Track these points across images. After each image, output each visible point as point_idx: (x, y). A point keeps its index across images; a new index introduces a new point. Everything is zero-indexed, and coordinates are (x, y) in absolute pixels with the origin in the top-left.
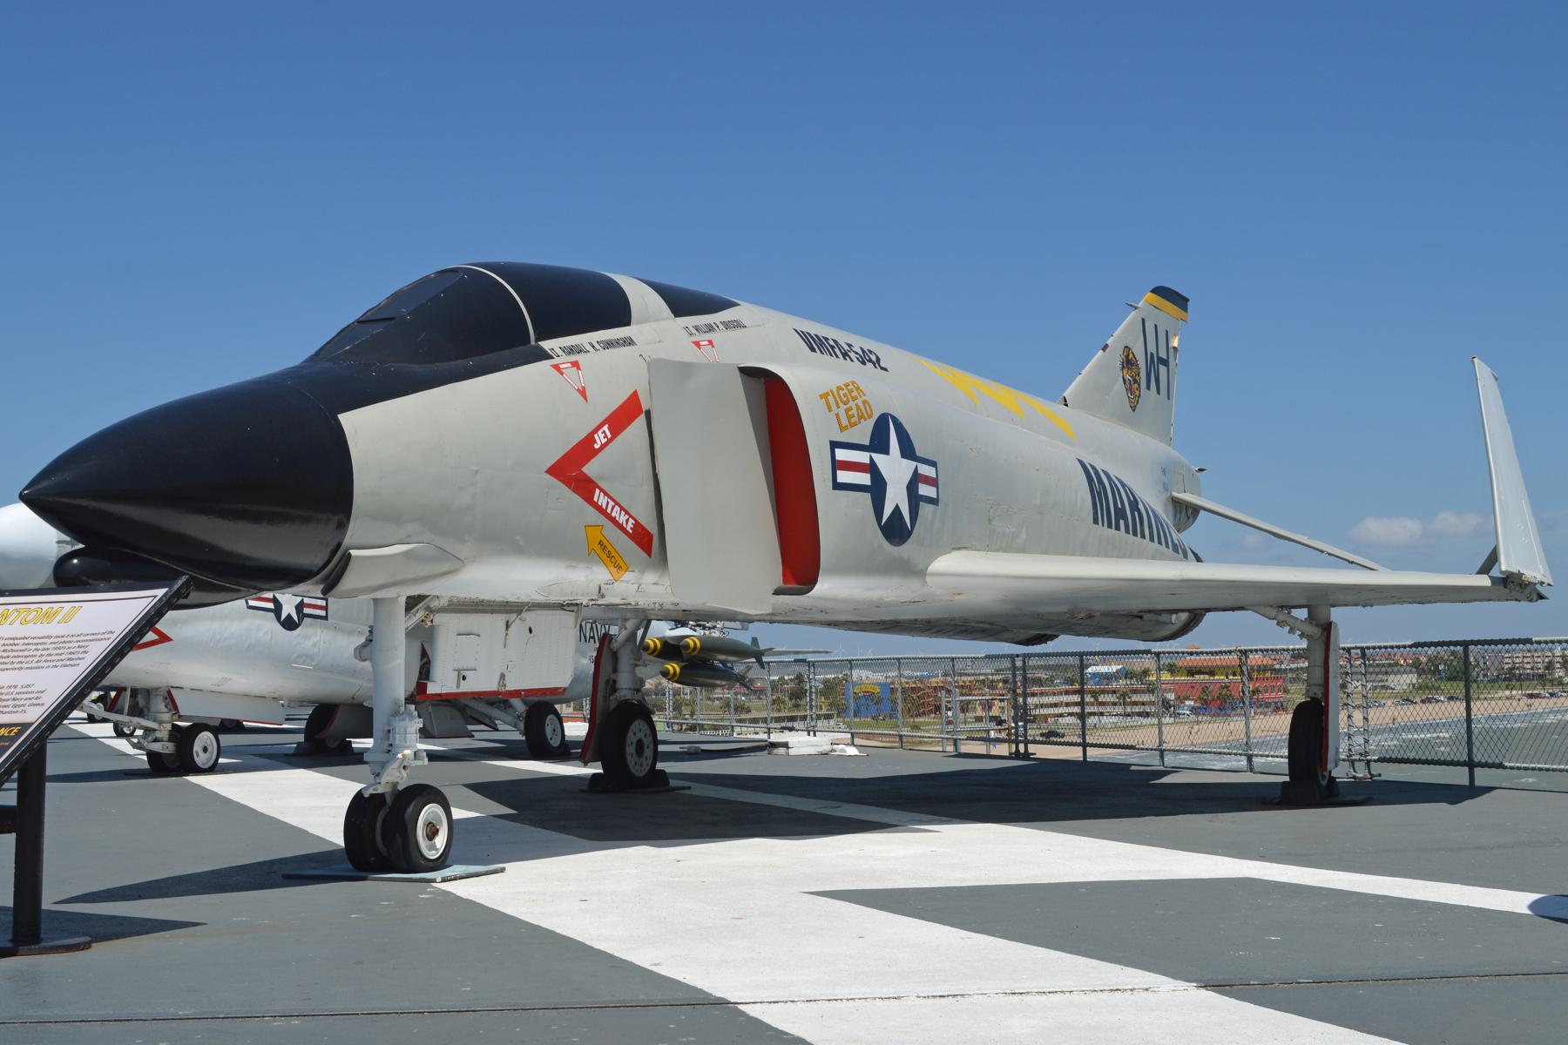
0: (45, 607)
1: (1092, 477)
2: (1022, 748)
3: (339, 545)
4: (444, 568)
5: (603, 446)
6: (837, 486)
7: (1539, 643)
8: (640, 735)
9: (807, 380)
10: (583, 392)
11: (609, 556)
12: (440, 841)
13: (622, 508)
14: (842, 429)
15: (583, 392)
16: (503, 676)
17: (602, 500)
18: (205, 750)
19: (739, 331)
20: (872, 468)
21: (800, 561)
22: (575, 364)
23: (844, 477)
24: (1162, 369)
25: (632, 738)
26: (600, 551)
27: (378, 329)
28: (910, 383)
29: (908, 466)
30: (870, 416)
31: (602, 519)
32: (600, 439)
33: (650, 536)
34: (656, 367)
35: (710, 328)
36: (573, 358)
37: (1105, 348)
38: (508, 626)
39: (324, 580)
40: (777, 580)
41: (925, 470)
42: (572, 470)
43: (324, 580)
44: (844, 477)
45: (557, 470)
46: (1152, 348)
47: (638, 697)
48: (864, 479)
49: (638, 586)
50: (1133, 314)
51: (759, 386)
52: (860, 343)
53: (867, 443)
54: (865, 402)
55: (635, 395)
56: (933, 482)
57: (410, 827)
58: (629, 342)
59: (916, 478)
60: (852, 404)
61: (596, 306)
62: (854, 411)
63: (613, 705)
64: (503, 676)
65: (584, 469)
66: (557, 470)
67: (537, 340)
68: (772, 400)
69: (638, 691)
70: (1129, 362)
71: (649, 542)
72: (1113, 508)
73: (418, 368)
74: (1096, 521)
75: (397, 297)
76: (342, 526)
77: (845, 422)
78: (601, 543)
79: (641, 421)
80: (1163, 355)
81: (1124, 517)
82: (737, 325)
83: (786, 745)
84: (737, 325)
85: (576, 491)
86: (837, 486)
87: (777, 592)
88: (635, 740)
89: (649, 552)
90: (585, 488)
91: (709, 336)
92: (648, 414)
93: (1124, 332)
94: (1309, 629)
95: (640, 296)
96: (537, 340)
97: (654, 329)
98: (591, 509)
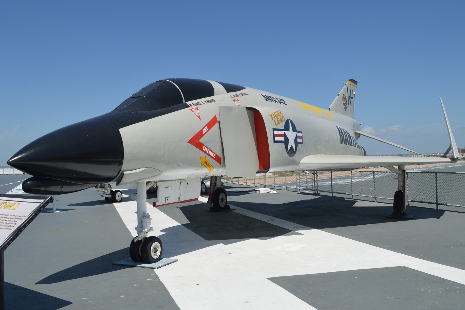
0: (11, 202)
1: (340, 130)
2: (316, 192)
3: (120, 170)
4: (156, 174)
5: (206, 133)
6: (275, 142)
7: (457, 173)
8: (222, 197)
9: (266, 110)
10: (199, 117)
11: (208, 165)
12: (158, 253)
13: (212, 151)
14: (276, 125)
15: (199, 117)
16: (179, 198)
17: (205, 149)
18: (119, 196)
19: (246, 96)
20: (285, 136)
21: (264, 164)
22: (197, 108)
23: (277, 139)
24: (352, 100)
25: (220, 198)
26: (205, 164)
27: (134, 100)
28: (294, 109)
29: (295, 134)
30: (284, 120)
31: (206, 155)
32: (204, 131)
33: (220, 158)
34: (222, 109)
35: (238, 96)
36: (196, 107)
37: (339, 95)
38: (180, 183)
39: (117, 180)
40: (258, 168)
41: (299, 134)
42: (196, 141)
43: (117, 180)
44: (277, 139)
45: (191, 142)
46: (349, 95)
47: (222, 187)
48: (282, 139)
49: (217, 172)
50: (345, 86)
51: (252, 112)
52: (279, 97)
53: (283, 128)
54: (282, 116)
55: (215, 117)
56: (301, 138)
57: (148, 250)
58: (214, 101)
59: (297, 137)
60: (279, 117)
61: (205, 90)
62: (279, 119)
63: (216, 189)
64: (179, 198)
65: (200, 140)
66: (191, 142)
67: (185, 102)
68: (256, 117)
69: (222, 185)
70: (344, 99)
71: (220, 160)
72: (345, 139)
73: (147, 112)
74: (341, 143)
75: (143, 90)
76: (121, 163)
77: (277, 123)
78: (205, 162)
79: (217, 124)
80: (352, 96)
81: (348, 141)
82: (245, 94)
83: (259, 191)
84: (245, 94)
85: (197, 147)
86: (275, 142)
87: (258, 172)
88: (221, 198)
89: (220, 163)
90: (200, 146)
91: (238, 98)
92: (219, 122)
93: (343, 91)
94: (399, 172)
95: (217, 87)
96: (185, 102)
97: (221, 97)
98: (202, 152)
